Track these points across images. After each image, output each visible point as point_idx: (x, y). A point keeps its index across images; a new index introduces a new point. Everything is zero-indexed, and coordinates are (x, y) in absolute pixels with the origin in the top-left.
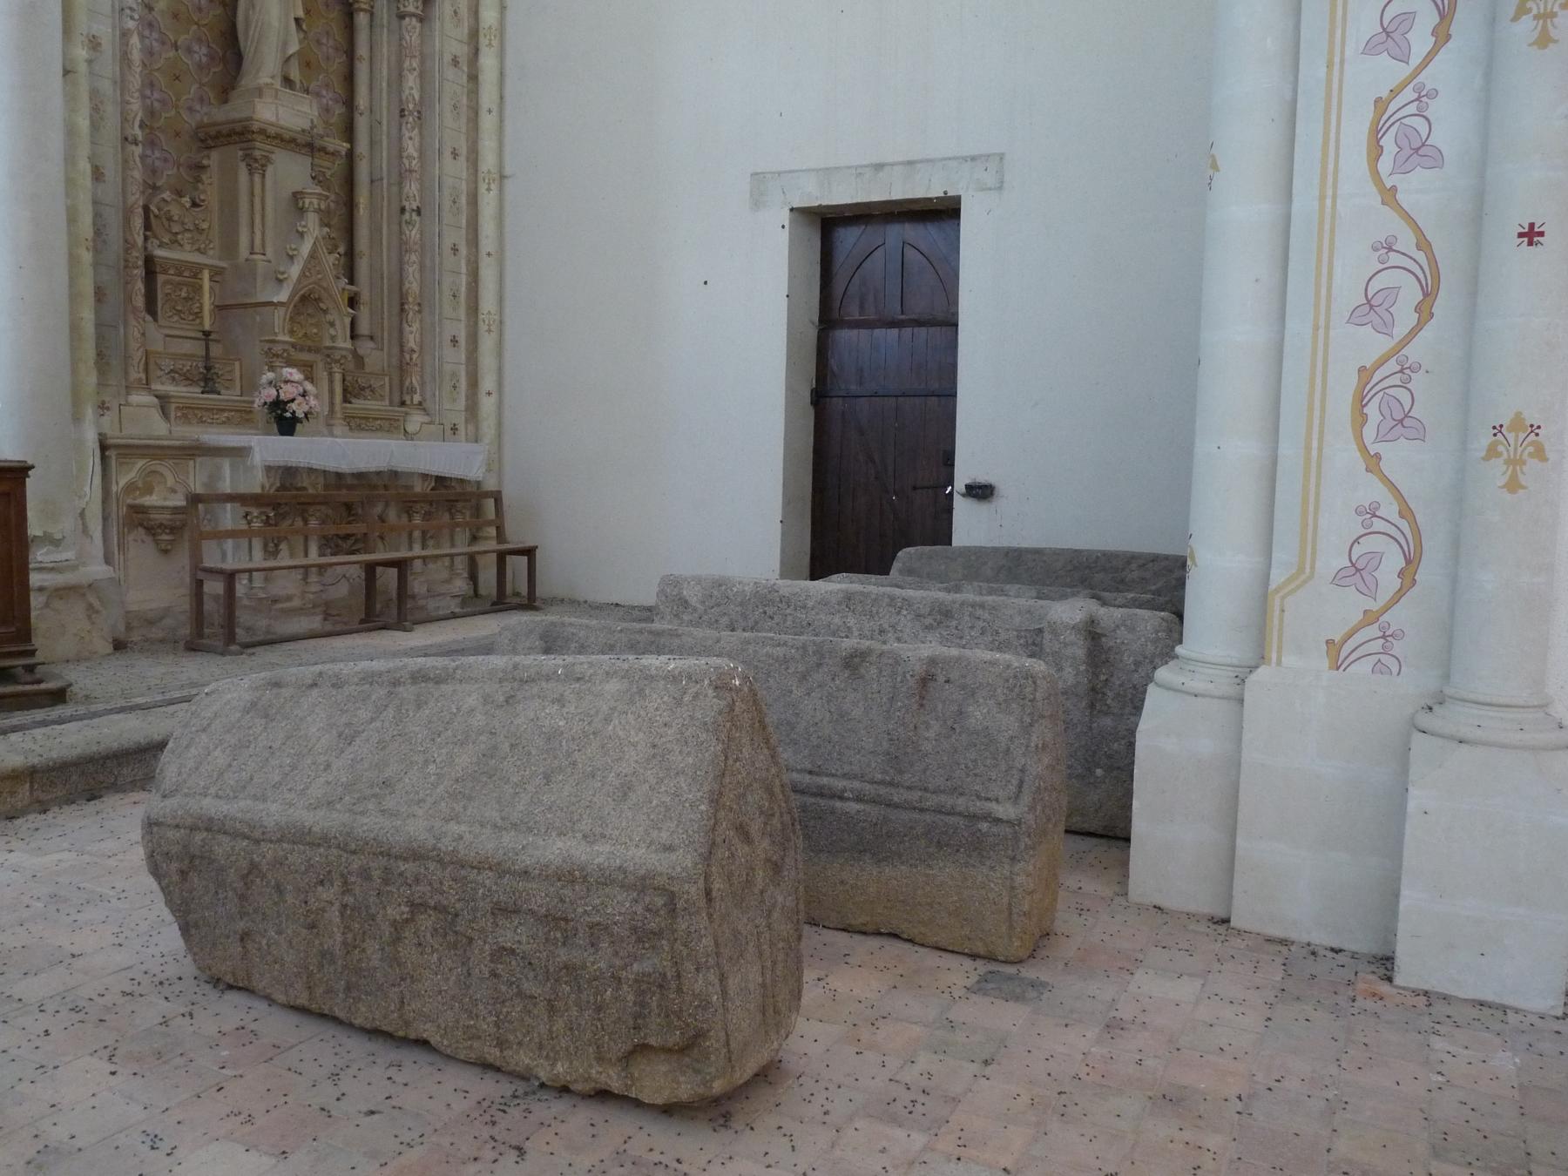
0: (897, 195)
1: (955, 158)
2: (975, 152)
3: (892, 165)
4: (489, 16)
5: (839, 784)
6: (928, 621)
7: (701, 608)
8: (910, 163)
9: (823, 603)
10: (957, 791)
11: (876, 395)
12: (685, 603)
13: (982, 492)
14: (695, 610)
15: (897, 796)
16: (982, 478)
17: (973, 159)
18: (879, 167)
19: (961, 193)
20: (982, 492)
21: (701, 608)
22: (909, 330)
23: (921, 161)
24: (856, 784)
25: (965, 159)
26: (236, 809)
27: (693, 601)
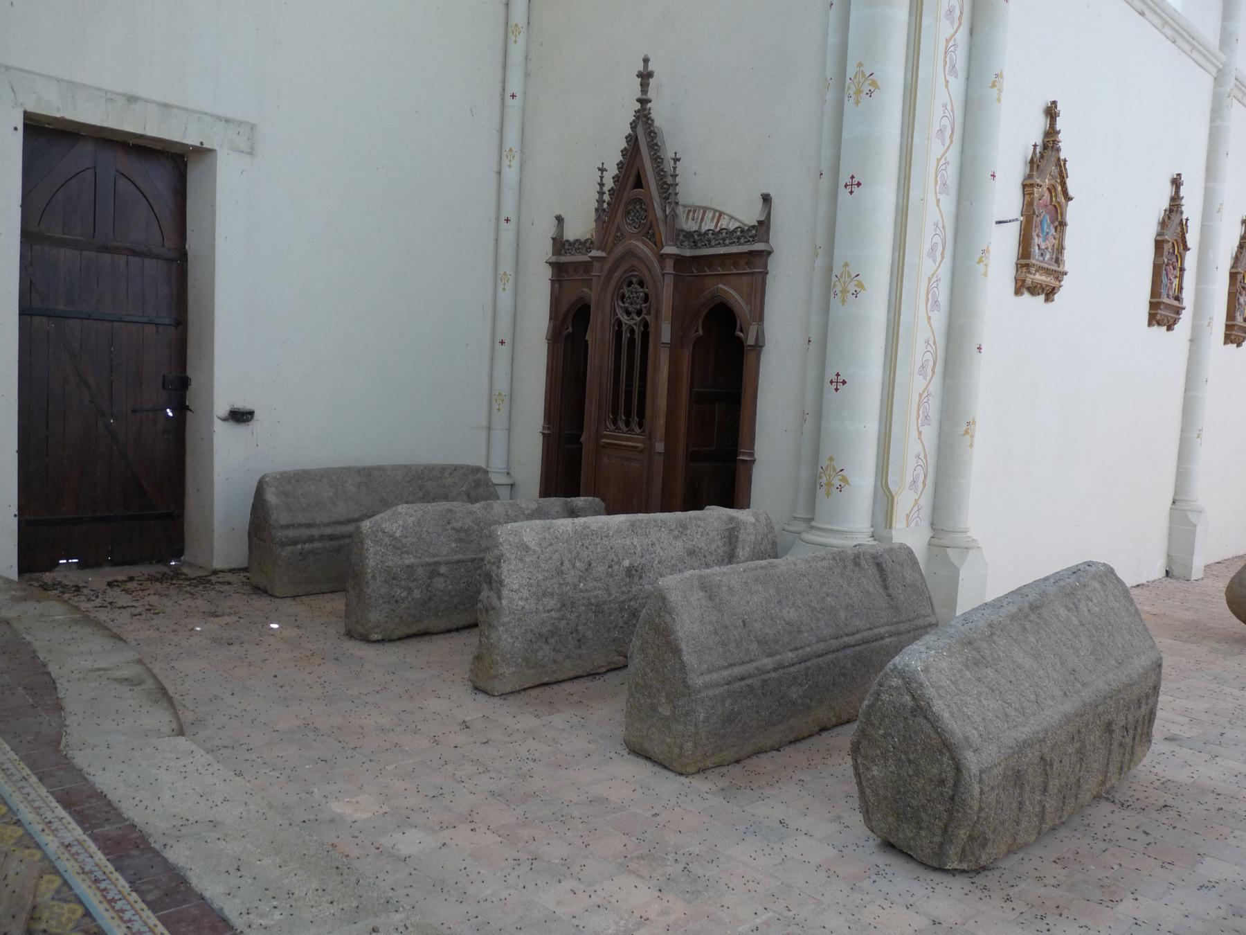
0: (152, 131)
1: (213, 116)
2: (229, 114)
3: (146, 101)
4: (519, 13)
5: (882, 630)
6: (676, 533)
7: (538, 550)
8: (166, 106)
9: (619, 531)
10: (918, 617)
11: (89, 318)
12: (527, 548)
13: (240, 416)
14: (535, 552)
15: (902, 627)
16: (242, 405)
17: (227, 121)
18: (132, 99)
19: (216, 147)
20: (240, 416)
21: (538, 550)
22: (124, 258)
23: (178, 108)
24: (887, 628)
25: (219, 118)
26: (1024, 733)
27: (532, 545)
